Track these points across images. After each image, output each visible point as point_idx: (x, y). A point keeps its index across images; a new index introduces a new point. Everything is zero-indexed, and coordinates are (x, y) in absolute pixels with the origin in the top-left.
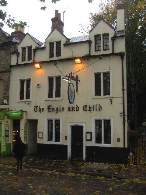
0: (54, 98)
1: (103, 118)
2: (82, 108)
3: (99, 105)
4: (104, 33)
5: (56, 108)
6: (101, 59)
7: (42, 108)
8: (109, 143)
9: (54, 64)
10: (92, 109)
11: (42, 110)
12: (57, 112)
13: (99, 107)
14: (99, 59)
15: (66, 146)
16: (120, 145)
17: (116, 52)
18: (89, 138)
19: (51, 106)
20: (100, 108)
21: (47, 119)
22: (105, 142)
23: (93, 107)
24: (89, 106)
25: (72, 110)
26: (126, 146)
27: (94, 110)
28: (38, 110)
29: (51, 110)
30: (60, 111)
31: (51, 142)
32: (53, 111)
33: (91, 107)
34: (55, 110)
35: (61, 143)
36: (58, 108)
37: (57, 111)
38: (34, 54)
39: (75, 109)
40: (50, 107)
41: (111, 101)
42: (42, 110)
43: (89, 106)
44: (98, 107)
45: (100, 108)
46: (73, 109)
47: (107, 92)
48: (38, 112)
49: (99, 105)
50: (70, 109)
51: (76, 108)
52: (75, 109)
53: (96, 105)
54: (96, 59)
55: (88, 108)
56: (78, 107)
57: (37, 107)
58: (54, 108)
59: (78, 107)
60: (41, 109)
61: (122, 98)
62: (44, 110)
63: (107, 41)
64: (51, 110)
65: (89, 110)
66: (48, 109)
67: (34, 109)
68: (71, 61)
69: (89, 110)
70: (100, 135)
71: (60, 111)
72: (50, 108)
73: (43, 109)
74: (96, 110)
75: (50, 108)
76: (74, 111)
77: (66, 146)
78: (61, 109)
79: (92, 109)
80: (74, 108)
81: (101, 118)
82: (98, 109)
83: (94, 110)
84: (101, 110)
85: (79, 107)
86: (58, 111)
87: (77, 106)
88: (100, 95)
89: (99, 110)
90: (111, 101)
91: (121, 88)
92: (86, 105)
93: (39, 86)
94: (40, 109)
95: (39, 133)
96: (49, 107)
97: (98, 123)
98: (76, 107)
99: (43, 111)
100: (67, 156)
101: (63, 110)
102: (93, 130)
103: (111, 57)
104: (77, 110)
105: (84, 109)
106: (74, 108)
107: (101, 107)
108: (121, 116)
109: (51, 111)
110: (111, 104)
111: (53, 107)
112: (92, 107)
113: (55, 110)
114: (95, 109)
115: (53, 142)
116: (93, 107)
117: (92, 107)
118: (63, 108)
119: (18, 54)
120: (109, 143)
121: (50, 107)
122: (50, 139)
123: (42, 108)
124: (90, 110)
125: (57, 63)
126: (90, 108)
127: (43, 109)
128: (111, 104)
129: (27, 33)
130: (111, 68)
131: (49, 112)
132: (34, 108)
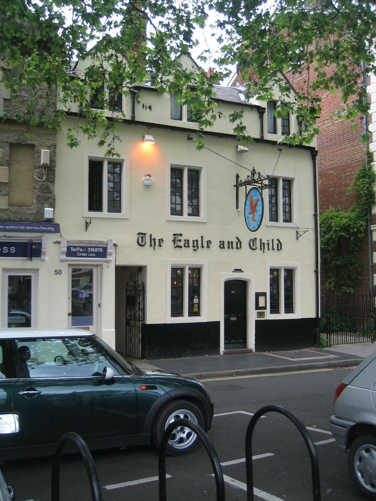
0: (185, 217)
3: (278, 240)
5: (193, 241)
8: (198, 314)
13: (278, 244)
15: (218, 323)
16: (311, 314)
18: (261, 300)
19: (181, 235)
22: (191, 314)
23: (268, 244)
24: (151, 235)
26: (320, 317)
27: (269, 249)
28: (259, 247)
32: (187, 245)
33: (264, 244)
34: (191, 244)
35: (203, 318)
36: (197, 241)
37: (196, 246)
40: (179, 238)
43: (151, 235)
44: (276, 242)
46: (195, 245)
47: (288, 219)
48: (258, 251)
49: (237, 238)
50: (208, 245)
51: (237, 243)
53: (273, 240)
56: (239, 241)
57: (145, 234)
64: (182, 244)
70: (25, 301)
72: (180, 240)
73: (161, 241)
74: (203, 247)
75: (180, 240)
77: (218, 323)
78: (205, 244)
82: (275, 247)
83: (269, 249)
85: (241, 241)
86: (198, 247)
87: (237, 238)
90: (87, 225)
92: (256, 239)
94: (153, 240)
96: (176, 238)
98: (235, 241)
100: (219, 350)
102: (267, 289)
105: (140, 241)
106: (232, 242)
107: (240, 242)
109: (181, 247)
110: (86, 231)
112: (266, 242)
113: (191, 244)
114: (271, 247)
115: (186, 319)
117: (266, 242)
118: (209, 242)
119: (359, 331)
120: (198, 314)
121: (179, 238)
122: (177, 310)
126: (262, 244)
131: (279, 251)
132: (136, 237)
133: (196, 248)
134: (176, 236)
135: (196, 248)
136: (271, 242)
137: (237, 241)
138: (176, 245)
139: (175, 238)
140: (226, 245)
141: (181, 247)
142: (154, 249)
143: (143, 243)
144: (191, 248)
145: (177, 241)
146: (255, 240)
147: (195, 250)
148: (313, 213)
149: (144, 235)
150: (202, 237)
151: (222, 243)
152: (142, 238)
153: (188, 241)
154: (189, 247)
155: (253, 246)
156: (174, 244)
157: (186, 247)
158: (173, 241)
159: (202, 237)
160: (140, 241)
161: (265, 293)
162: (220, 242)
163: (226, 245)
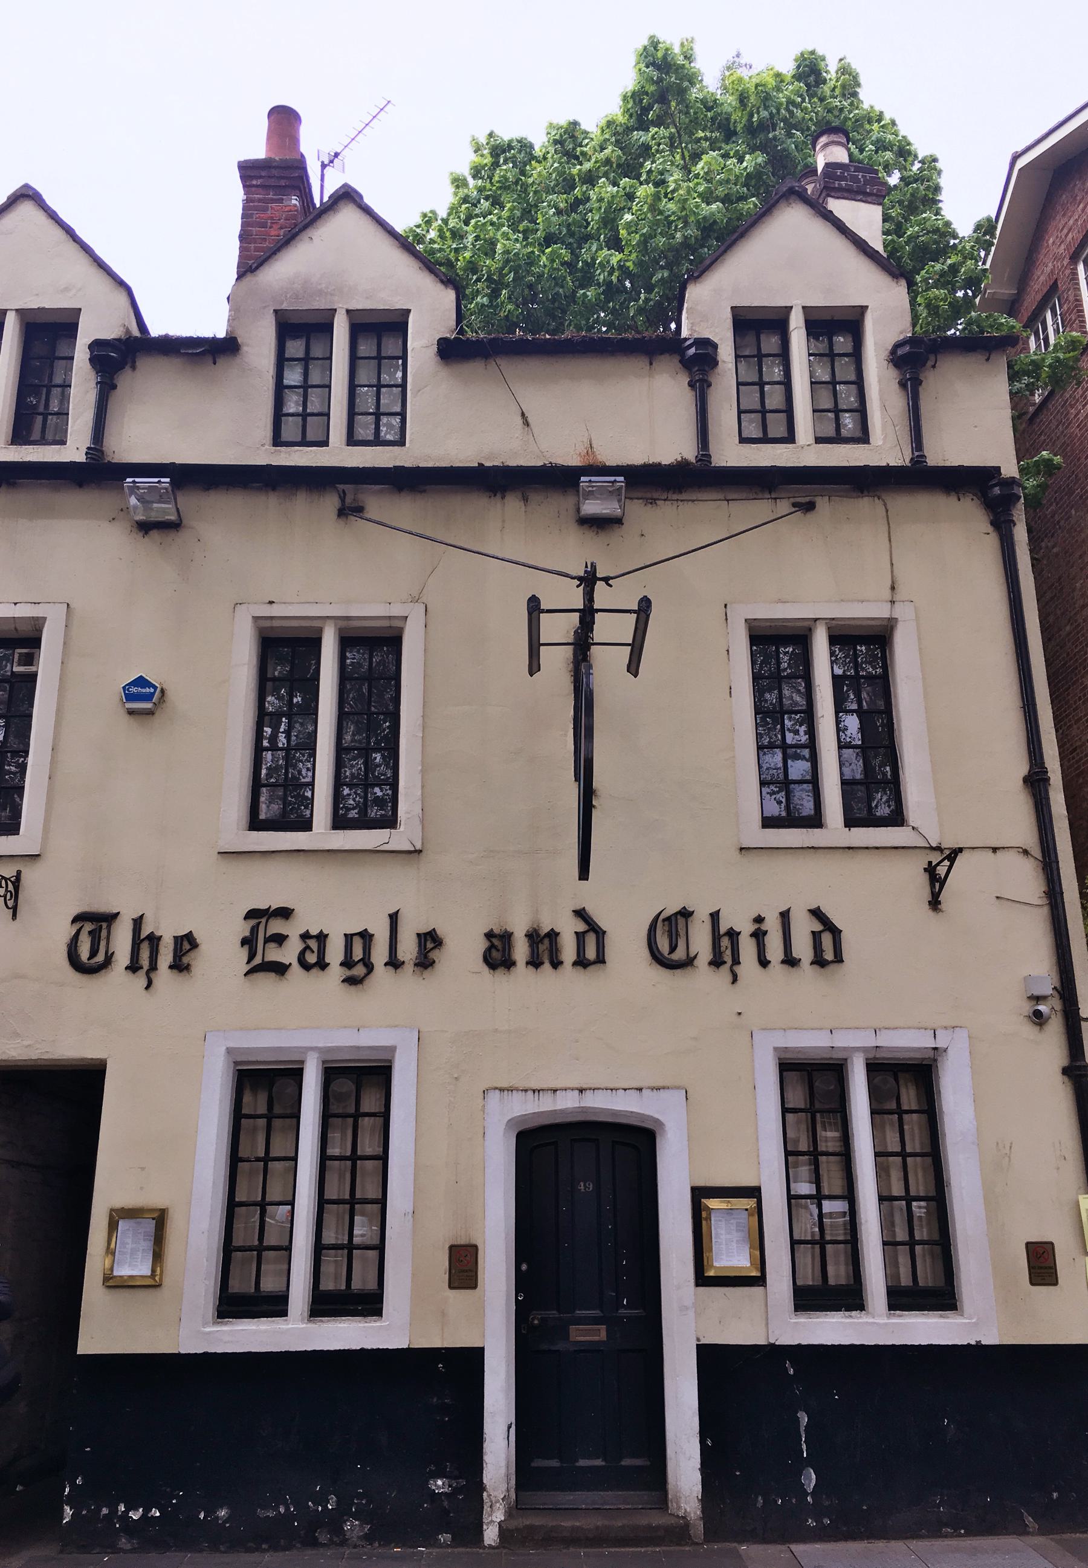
1: (867, 1040)
2: (646, 952)
3: (817, 913)
4: (818, 300)
5: (349, 938)
6: (809, 507)
7: (168, 933)
9: (330, 503)
10: (747, 949)
11: (166, 957)
12: (352, 981)
13: (816, 936)
14: (784, 506)
17: (934, 459)
19: (285, 913)
20: (827, 940)
21: (229, 1051)
23: (759, 936)
24: (715, 917)
25: (535, 963)
27: (764, 963)
28: (122, 957)
29: (288, 954)
30: (394, 963)
31: (857, 1318)
34: (335, 953)
36: (366, 936)
38: (106, 389)
39: (568, 951)
40: (276, 926)
41: (936, 881)
42: (166, 957)
43: (715, 917)
44: (803, 929)
45: (827, 940)
46: (358, 953)
49: (581, 914)
51: (580, 937)
52: (568, 951)
53: (785, 916)
54: (760, 508)
55: (700, 941)
57: (111, 918)
58: (322, 938)
59: (593, 927)
60: (154, 940)
61: (1037, 852)
62: (201, 961)
63: (315, 378)
64: (288, 954)
65: (133, 967)
66: (248, 942)
67: (75, 939)
68: (499, 495)
69: (716, 962)
71: (394, 963)
72: (280, 939)
73: (186, 943)
74: (790, 961)
75: (280, 939)
76: (556, 964)
78: (408, 949)
79: (747, 949)
80: (553, 935)
81: (843, 1040)
82: (803, 948)
83: (764, 963)
84: (839, 959)
85: (603, 924)
86: (370, 968)
87: (581, 914)
88: (306, 825)
89: (819, 962)
90: (936, 881)
91: (1021, 768)
92: (686, 914)
93: (148, 698)
95: (113, 1226)
97: (254, 1103)
98: (568, 929)
99: (179, 966)
101: (425, 963)
103: (903, 503)
104: (581, 962)
105: (663, 944)
106: (553, 935)
107: (836, 932)
108: (1038, 1018)
109: (280, 969)
110: (935, 903)
111: (307, 921)
113: (335, 953)
116: (759, 936)
117: (745, 928)
123: (168, 933)
124: (145, 962)
125: (822, 503)
127: (186, 943)
128: (935, 903)
129: (347, 196)
130: (902, 593)
131: (267, 980)
132: (64, 931)
133: (359, 970)
134: (264, 920)
135: (359, 970)
136: (773, 925)
137: (581, 927)
138: (258, 960)
139: (254, 930)
140: (521, 951)
141: (280, 969)
142: (735, 979)
143: (100, 958)
144: (336, 972)
145: (267, 940)
146: (681, 921)
147: (351, 981)
148: (1023, 769)
149: (104, 925)
150: (394, 918)
151: (313, 943)
152: (95, 935)
153: (322, 938)
154: (322, 965)
155: (673, 949)
156: (251, 956)
157: (306, 966)
158: (244, 942)
159: (394, 918)
160: (663, 944)
161: (754, 1192)
162: (489, 935)
163: (521, 951)
